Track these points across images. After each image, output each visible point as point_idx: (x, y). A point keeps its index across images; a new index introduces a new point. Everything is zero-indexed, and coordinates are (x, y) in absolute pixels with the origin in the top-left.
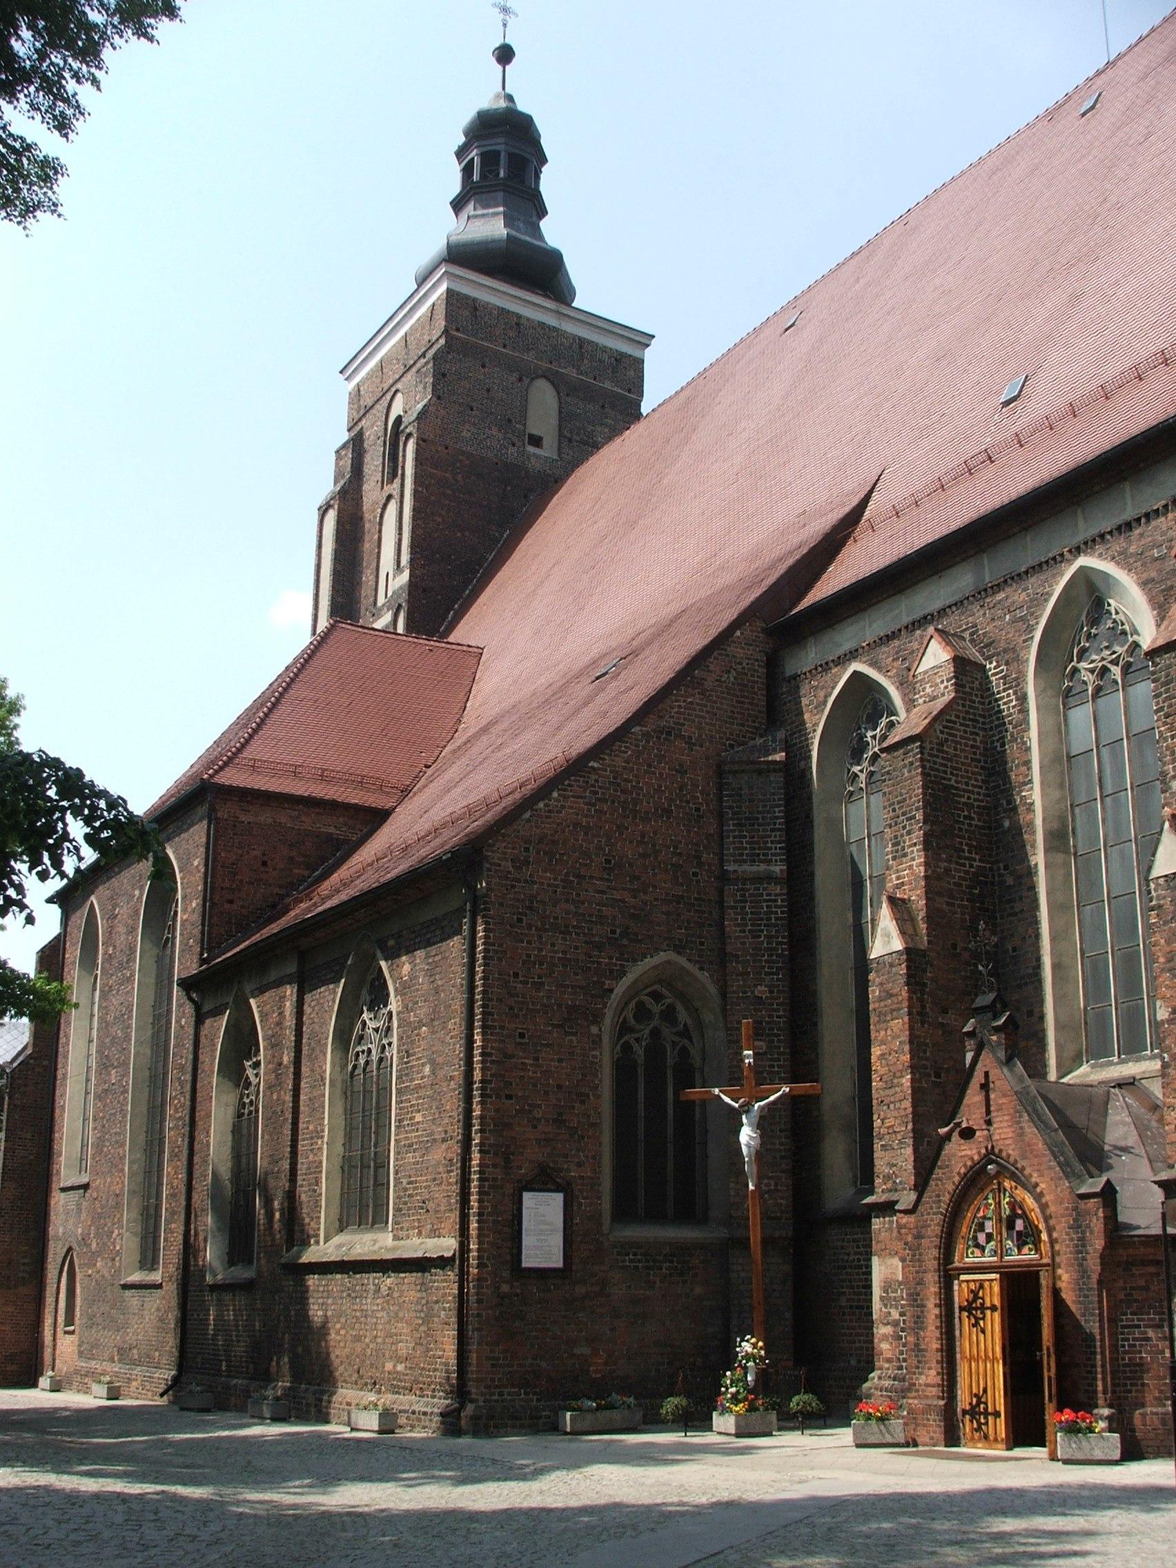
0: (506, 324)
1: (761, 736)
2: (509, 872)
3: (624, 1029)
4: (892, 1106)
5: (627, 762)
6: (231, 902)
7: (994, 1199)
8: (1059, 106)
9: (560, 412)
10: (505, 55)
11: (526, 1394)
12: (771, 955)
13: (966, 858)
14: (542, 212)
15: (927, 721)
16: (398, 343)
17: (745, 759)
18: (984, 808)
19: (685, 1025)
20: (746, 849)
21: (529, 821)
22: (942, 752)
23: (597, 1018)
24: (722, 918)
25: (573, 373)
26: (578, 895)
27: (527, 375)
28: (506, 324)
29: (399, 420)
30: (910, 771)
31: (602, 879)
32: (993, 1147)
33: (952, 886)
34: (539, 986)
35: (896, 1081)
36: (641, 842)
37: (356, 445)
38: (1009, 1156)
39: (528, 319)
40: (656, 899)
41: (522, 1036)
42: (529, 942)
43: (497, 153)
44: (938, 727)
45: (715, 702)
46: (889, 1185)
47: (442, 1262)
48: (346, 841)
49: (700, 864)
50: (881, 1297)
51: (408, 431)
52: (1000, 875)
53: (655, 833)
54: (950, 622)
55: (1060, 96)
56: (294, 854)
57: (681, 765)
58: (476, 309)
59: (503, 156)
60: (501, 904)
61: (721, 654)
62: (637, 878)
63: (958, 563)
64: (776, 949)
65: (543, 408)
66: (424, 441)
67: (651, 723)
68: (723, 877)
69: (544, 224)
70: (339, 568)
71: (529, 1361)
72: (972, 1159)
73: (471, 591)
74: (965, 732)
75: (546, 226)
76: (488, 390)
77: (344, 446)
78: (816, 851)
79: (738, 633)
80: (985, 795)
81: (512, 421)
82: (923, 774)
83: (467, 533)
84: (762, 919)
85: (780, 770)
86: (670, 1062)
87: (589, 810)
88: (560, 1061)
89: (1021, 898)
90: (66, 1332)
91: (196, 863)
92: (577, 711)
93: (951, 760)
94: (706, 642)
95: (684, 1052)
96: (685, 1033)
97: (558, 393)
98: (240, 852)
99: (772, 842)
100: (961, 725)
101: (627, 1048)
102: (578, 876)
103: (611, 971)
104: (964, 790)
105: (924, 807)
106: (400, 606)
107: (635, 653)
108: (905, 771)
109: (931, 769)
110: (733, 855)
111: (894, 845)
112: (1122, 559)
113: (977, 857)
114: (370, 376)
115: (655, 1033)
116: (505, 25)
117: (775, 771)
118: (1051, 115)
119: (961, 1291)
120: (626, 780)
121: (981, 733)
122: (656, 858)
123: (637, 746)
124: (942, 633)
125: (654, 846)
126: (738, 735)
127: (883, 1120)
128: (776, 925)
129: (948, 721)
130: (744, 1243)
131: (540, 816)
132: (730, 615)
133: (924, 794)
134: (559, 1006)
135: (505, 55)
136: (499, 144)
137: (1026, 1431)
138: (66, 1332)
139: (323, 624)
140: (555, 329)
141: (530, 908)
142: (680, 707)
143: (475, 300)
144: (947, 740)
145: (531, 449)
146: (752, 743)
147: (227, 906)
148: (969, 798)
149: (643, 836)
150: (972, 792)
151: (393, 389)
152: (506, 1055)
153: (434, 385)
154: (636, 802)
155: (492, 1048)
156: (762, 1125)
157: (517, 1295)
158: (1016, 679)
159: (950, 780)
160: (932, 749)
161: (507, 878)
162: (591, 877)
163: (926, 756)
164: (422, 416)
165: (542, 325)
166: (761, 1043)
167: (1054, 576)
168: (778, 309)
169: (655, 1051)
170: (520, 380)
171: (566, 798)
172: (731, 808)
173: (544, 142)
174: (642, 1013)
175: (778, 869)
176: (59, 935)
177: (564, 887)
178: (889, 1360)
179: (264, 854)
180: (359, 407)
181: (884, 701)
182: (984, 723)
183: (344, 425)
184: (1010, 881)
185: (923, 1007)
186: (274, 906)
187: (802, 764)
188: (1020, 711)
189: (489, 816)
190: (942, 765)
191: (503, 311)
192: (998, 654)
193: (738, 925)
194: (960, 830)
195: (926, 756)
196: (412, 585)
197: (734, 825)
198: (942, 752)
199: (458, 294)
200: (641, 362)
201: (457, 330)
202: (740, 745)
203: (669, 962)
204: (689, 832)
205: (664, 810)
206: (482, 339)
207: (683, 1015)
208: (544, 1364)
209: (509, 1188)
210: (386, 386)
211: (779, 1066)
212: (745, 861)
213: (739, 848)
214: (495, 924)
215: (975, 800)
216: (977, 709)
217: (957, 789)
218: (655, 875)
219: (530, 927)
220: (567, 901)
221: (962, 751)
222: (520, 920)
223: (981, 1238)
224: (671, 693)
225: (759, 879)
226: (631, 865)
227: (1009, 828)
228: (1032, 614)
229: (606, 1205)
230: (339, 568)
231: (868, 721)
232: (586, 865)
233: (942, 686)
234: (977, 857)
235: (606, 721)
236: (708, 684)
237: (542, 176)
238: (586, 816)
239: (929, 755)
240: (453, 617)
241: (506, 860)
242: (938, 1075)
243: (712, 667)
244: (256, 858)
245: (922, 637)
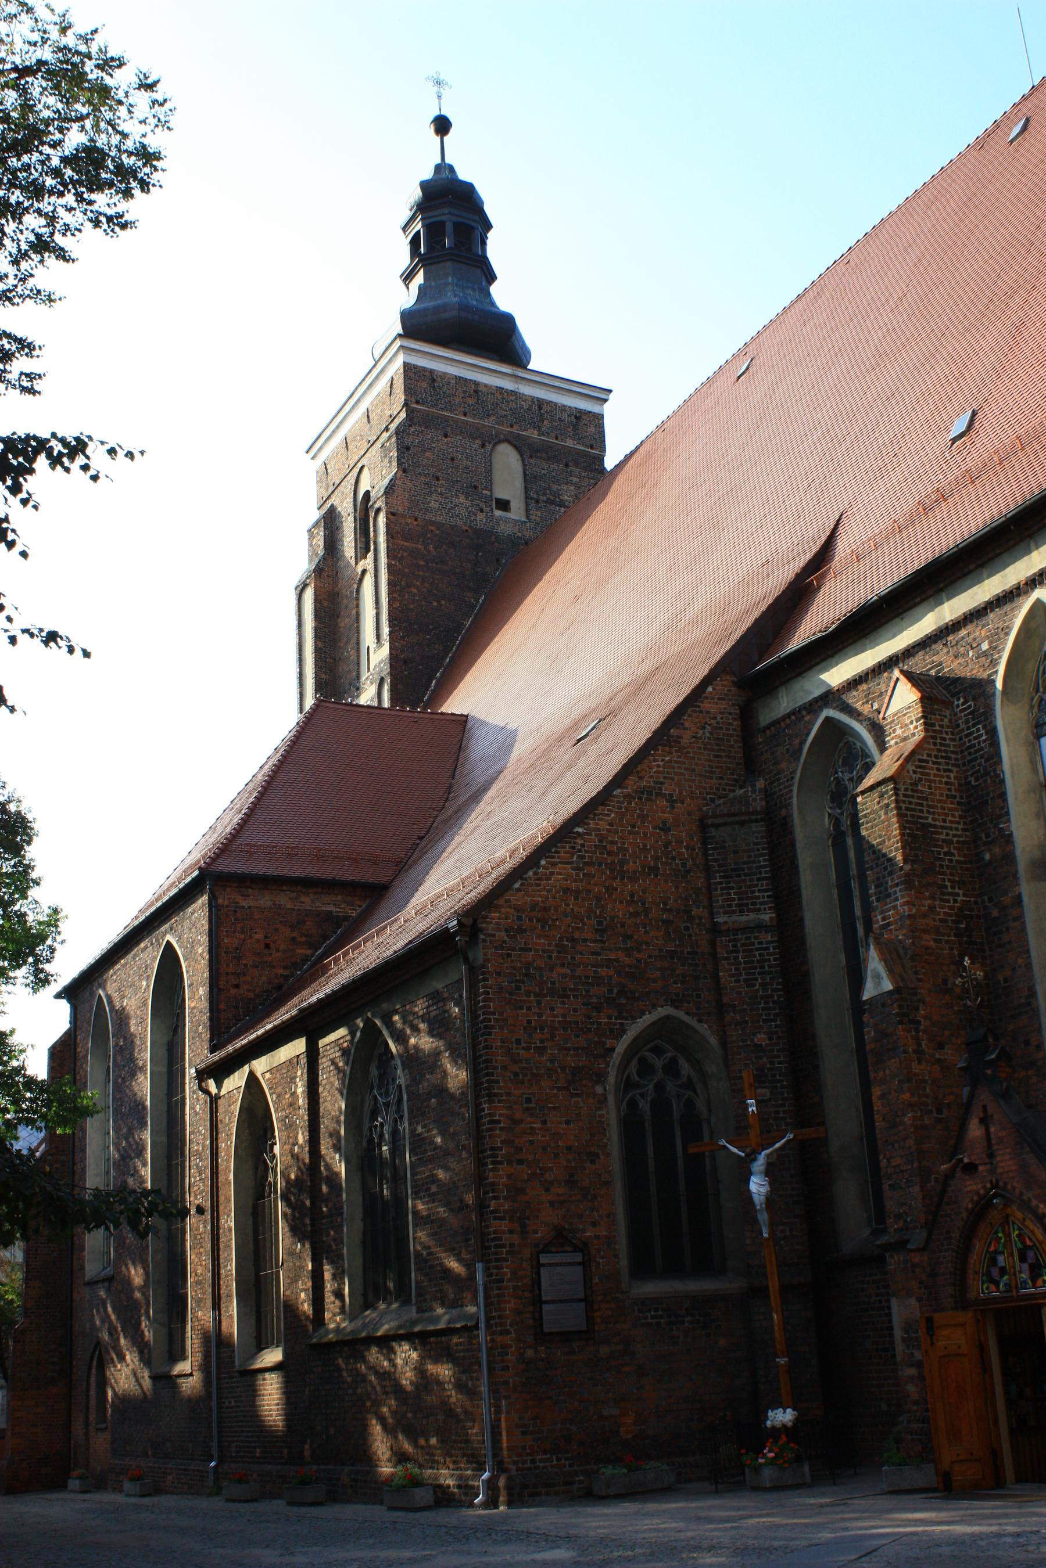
0: (464, 392)
1: (741, 787)
2: (504, 942)
3: (627, 1085)
4: (896, 1145)
5: (611, 824)
6: (237, 986)
7: (1003, 1232)
8: (988, 134)
9: (525, 473)
10: (442, 125)
11: (559, 1459)
12: (766, 1003)
13: (949, 894)
15: (899, 762)
16: (360, 419)
17: (725, 812)
18: (963, 843)
19: (689, 1077)
20: (734, 900)
21: (518, 890)
22: (916, 791)
23: (600, 1077)
24: (716, 970)
25: (535, 434)
26: (573, 958)
28: (464, 392)
29: (367, 493)
30: (886, 813)
31: (595, 941)
32: (997, 1180)
33: (937, 923)
34: (541, 1051)
35: (898, 1120)
36: (633, 901)
37: (330, 521)
38: (1014, 1188)
39: (486, 386)
40: (650, 957)
41: (528, 1100)
42: (529, 1009)
43: (442, 224)
44: (911, 767)
45: (693, 758)
46: (901, 1224)
47: (547, 1302)
48: (346, 918)
49: (691, 918)
50: (903, 1339)
51: (376, 506)
52: (985, 908)
53: (644, 891)
54: (919, 664)
55: (988, 124)
56: (295, 934)
57: (664, 823)
58: (434, 381)
59: (450, 224)
60: (498, 974)
61: (695, 711)
62: (630, 937)
63: (918, 604)
64: (772, 996)
65: (508, 474)
66: (393, 514)
67: (632, 783)
68: (715, 930)
69: (494, 290)
70: (320, 645)
71: (559, 1426)
72: (978, 1194)
73: (452, 658)
74: (938, 770)
75: (496, 290)
76: (452, 459)
77: (316, 525)
78: (804, 897)
79: (710, 689)
80: (964, 830)
81: (478, 487)
82: (899, 815)
83: (443, 602)
84: (756, 968)
85: (762, 820)
86: (676, 1115)
87: (577, 875)
88: (567, 1122)
89: (1007, 929)
90: (98, 1430)
91: (200, 951)
92: (561, 775)
93: (926, 799)
94: (680, 699)
95: (690, 1105)
96: (689, 1085)
97: (521, 455)
98: (242, 936)
99: (759, 891)
100: (934, 763)
101: (633, 1104)
102: (573, 940)
103: (611, 1030)
104: (942, 827)
105: (903, 847)
106: (382, 680)
107: (613, 714)
108: (882, 812)
109: (907, 809)
110: (722, 907)
111: (877, 887)
113: (961, 892)
114: (335, 454)
115: (660, 1087)
116: (439, 97)
117: (756, 821)
118: (981, 143)
120: (612, 843)
121: (955, 769)
122: (646, 916)
123: (620, 808)
124: (909, 676)
125: (643, 904)
126: (717, 789)
127: (889, 1160)
128: (770, 973)
129: (920, 761)
130: (762, 1292)
131: (531, 885)
132: (703, 671)
133: (902, 835)
134: (563, 1069)
135: (442, 125)
136: (446, 215)
138: (98, 1430)
139: (309, 702)
140: (513, 393)
141: (527, 975)
142: (658, 766)
143: (432, 371)
144: (920, 780)
145: (498, 513)
146: (731, 795)
147: (233, 991)
148: (947, 834)
149: (632, 896)
150: (951, 829)
151: (359, 465)
152: (515, 1122)
153: (399, 460)
154: (622, 863)
155: (500, 1115)
156: (769, 1172)
157: (542, 1360)
158: (984, 713)
159: (927, 818)
160: (906, 790)
161: (503, 948)
162: (585, 940)
163: (901, 798)
164: (389, 490)
165: (500, 389)
166: (764, 1090)
167: (1012, 610)
168: (729, 357)
170: (483, 446)
171: (554, 864)
172: (716, 860)
173: (488, 209)
174: (646, 1068)
175: (767, 917)
176: (69, 1029)
177: (559, 952)
178: (916, 1403)
179: (266, 937)
180: (328, 486)
181: (858, 744)
182: (956, 759)
183: (314, 504)
184: (995, 913)
185: (919, 1044)
186: (279, 987)
187: (783, 812)
188: (991, 745)
189: (481, 889)
190: (917, 804)
191: (459, 379)
192: (965, 690)
193: (731, 976)
194: (941, 866)
195: (901, 798)
196: (393, 657)
197: (721, 877)
198: (916, 791)
199: (415, 367)
200: (600, 417)
201: (417, 402)
202: (720, 798)
203: (667, 1017)
204: (677, 887)
205: (650, 868)
206: (442, 409)
207: (685, 1068)
208: (574, 1428)
209: (527, 1253)
210: (352, 463)
211: (784, 1112)
212: (734, 912)
213: (728, 900)
214: (494, 993)
215: (954, 836)
216: (948, 746)
217: (935, 826)
218: (646, 932)
219: (528, 993)
220: (563, 965)
221: (936, 788)
222: (518, 988)
223: (995, 1273)
224: (650, 754)
225: (747, 929)
226: (623, 925)
227: (990, 861)
228: (995, 648)
229: (624, 1263)
230: (320, 645)
231: (844, 764)
232: (578, 928)
233: (912, 727)
234: (961, 892)
235: (589, 785)
236: (685, 741)
237: (488, 242)
238: (575, 881)
239: (905, 796)
240: (436, 685)
241: (499, 930)
242: (939, 1111)
243: (687, 725)
244: (258, 941)
245: (890, 678)
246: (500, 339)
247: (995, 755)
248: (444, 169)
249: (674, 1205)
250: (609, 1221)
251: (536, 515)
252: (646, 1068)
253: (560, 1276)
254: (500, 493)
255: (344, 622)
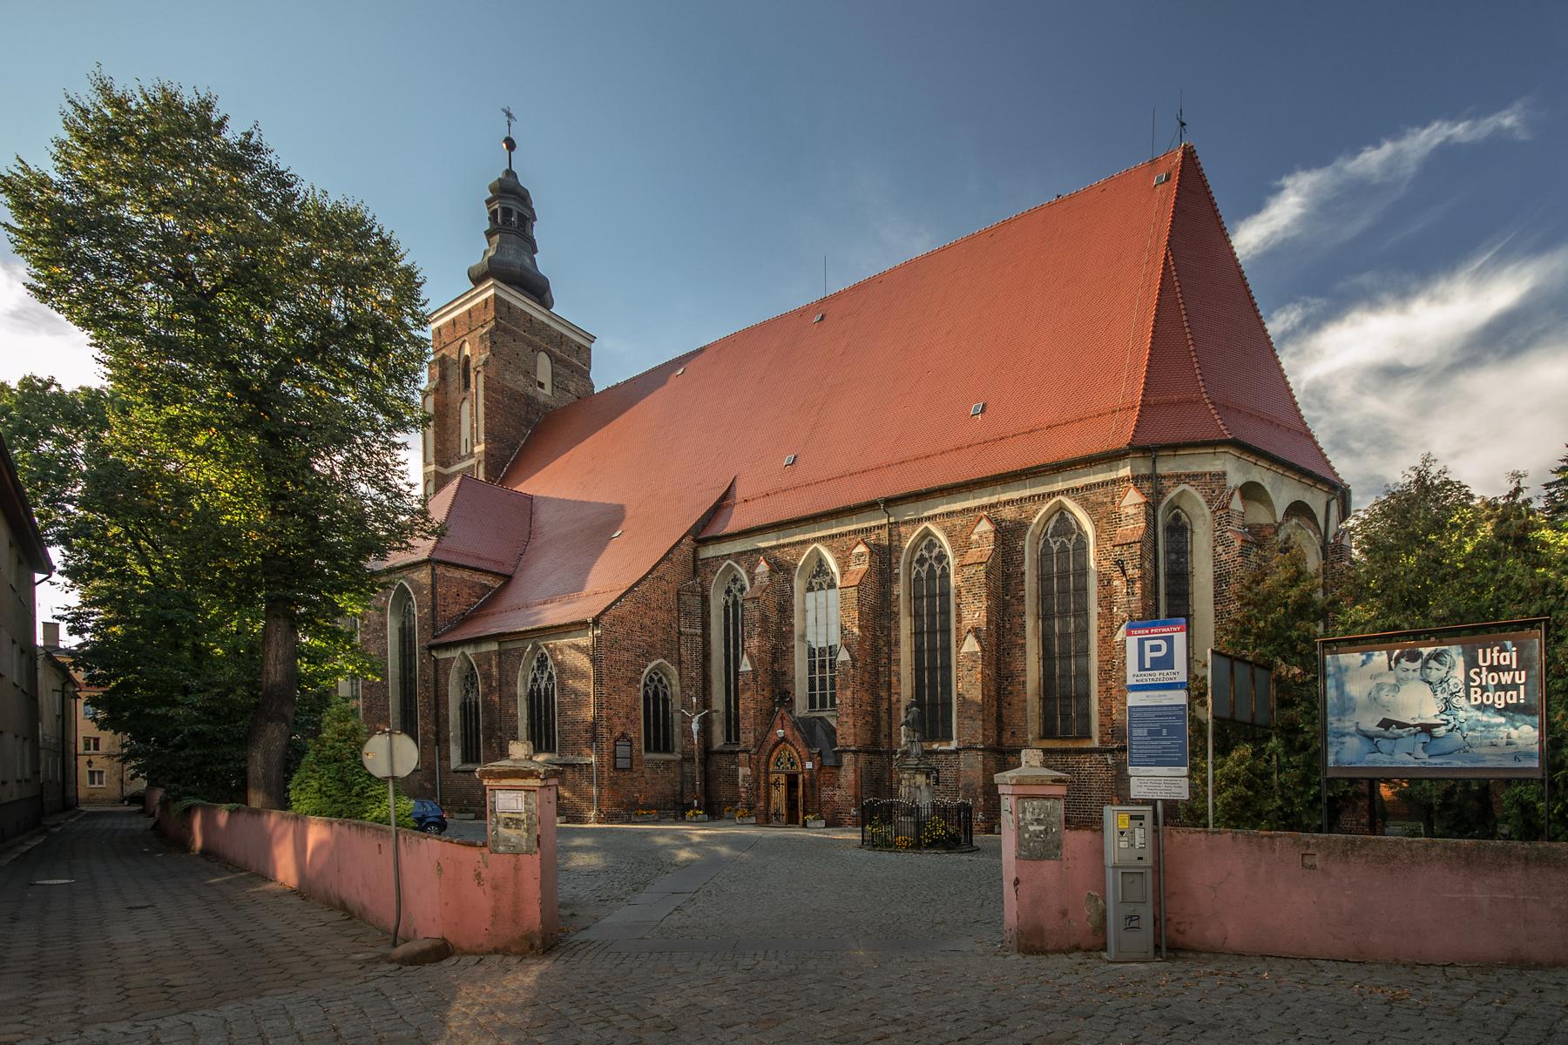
10: (511, 144)
14: (535, 251)
27: (536, 349)
68: (680, 633)
81: (529, 373)
112: (830, 548)
119: (773, 778)
136: (512, 204)
137: (792, 820)
169: (656, 693)
174: (652, 680)
175: (699, 631)
196: (486, 452)
246: (538, 290)
247: (792, 596)
248: (510, 173)
249: (659, 732)
250: (638, 732)
251: (557, 395)
252: (652, 680)
253: (623, 750)
254: (540, 378)
255: (450, 421)
